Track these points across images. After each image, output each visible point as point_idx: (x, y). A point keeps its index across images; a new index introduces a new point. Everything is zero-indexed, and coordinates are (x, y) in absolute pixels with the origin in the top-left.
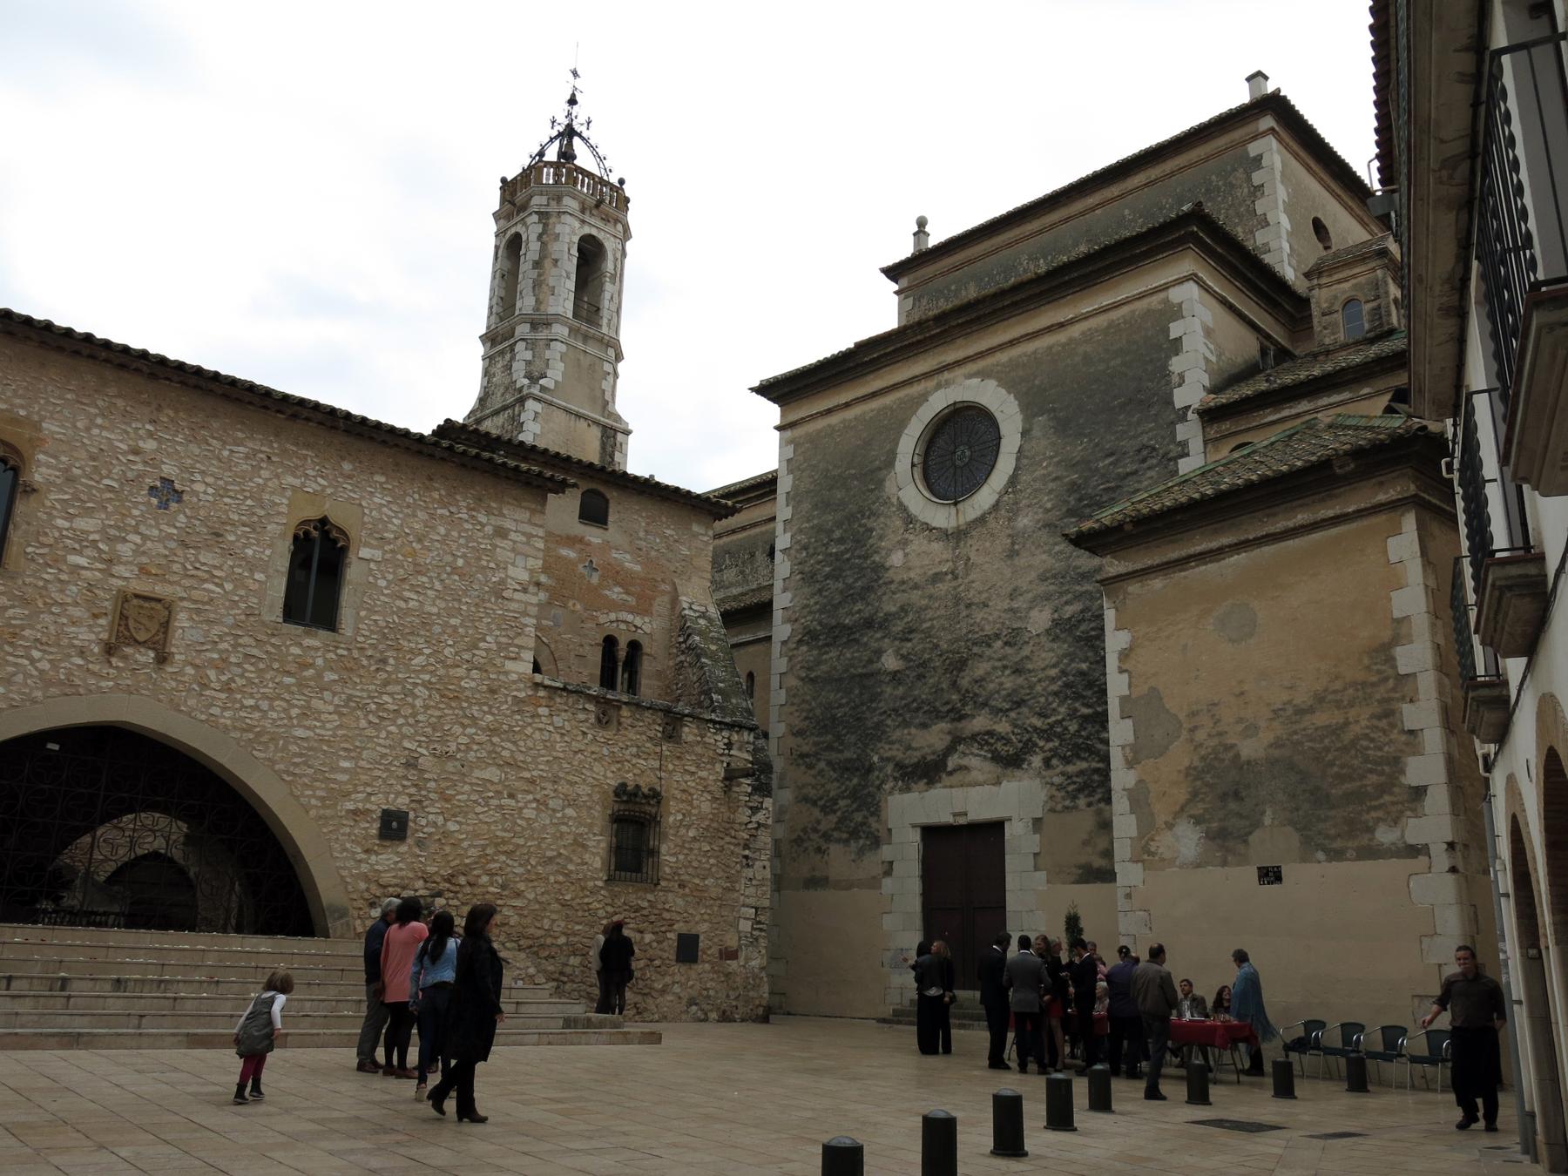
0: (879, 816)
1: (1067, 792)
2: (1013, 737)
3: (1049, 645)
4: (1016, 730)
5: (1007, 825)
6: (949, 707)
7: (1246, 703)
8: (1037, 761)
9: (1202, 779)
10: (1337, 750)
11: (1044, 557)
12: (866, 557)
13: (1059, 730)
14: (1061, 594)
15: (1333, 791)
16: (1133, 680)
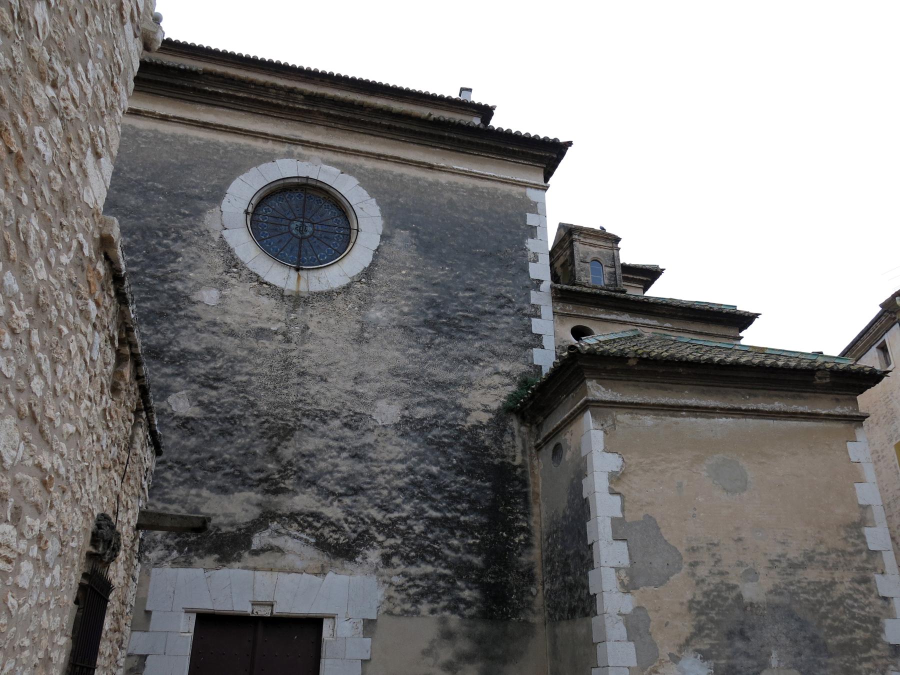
1: (408, 595)
2: (345, 525)
3: (396, 439)
4: (350, 519)
5: (327, 625)
6: (262, 475)
7: (744, 549)
8: (374, 556)
9: (707, 614)
10: (829, 604)
11: (397, 354)
12: (164, 280)
13: (402, 527)
14: (414, 394)
15: (829, 641)
16: (626, 504)
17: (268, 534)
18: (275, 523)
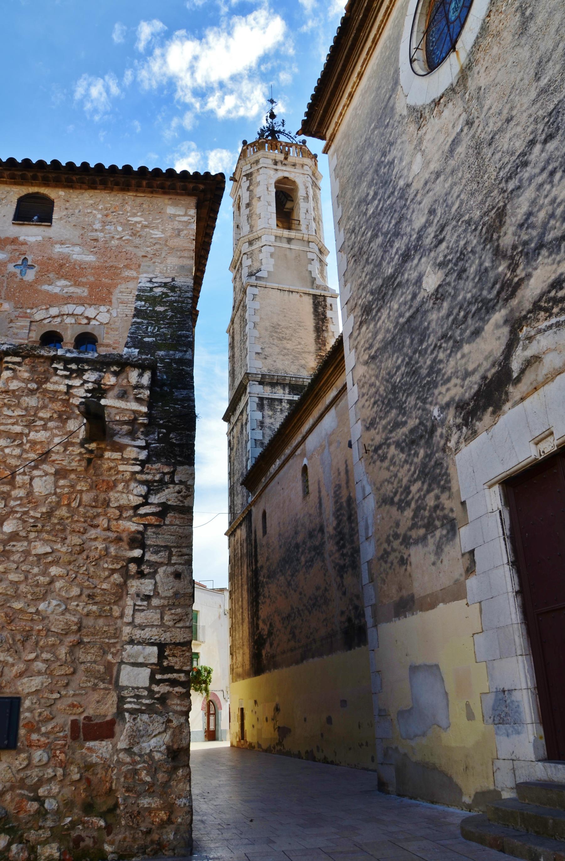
0: (449, 489)
17: (521, 348)
18: (525, 328)
